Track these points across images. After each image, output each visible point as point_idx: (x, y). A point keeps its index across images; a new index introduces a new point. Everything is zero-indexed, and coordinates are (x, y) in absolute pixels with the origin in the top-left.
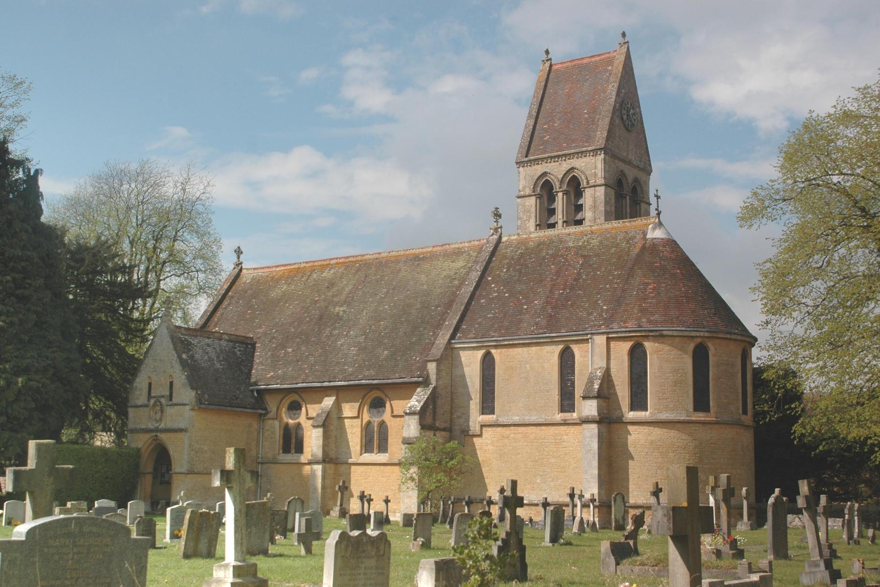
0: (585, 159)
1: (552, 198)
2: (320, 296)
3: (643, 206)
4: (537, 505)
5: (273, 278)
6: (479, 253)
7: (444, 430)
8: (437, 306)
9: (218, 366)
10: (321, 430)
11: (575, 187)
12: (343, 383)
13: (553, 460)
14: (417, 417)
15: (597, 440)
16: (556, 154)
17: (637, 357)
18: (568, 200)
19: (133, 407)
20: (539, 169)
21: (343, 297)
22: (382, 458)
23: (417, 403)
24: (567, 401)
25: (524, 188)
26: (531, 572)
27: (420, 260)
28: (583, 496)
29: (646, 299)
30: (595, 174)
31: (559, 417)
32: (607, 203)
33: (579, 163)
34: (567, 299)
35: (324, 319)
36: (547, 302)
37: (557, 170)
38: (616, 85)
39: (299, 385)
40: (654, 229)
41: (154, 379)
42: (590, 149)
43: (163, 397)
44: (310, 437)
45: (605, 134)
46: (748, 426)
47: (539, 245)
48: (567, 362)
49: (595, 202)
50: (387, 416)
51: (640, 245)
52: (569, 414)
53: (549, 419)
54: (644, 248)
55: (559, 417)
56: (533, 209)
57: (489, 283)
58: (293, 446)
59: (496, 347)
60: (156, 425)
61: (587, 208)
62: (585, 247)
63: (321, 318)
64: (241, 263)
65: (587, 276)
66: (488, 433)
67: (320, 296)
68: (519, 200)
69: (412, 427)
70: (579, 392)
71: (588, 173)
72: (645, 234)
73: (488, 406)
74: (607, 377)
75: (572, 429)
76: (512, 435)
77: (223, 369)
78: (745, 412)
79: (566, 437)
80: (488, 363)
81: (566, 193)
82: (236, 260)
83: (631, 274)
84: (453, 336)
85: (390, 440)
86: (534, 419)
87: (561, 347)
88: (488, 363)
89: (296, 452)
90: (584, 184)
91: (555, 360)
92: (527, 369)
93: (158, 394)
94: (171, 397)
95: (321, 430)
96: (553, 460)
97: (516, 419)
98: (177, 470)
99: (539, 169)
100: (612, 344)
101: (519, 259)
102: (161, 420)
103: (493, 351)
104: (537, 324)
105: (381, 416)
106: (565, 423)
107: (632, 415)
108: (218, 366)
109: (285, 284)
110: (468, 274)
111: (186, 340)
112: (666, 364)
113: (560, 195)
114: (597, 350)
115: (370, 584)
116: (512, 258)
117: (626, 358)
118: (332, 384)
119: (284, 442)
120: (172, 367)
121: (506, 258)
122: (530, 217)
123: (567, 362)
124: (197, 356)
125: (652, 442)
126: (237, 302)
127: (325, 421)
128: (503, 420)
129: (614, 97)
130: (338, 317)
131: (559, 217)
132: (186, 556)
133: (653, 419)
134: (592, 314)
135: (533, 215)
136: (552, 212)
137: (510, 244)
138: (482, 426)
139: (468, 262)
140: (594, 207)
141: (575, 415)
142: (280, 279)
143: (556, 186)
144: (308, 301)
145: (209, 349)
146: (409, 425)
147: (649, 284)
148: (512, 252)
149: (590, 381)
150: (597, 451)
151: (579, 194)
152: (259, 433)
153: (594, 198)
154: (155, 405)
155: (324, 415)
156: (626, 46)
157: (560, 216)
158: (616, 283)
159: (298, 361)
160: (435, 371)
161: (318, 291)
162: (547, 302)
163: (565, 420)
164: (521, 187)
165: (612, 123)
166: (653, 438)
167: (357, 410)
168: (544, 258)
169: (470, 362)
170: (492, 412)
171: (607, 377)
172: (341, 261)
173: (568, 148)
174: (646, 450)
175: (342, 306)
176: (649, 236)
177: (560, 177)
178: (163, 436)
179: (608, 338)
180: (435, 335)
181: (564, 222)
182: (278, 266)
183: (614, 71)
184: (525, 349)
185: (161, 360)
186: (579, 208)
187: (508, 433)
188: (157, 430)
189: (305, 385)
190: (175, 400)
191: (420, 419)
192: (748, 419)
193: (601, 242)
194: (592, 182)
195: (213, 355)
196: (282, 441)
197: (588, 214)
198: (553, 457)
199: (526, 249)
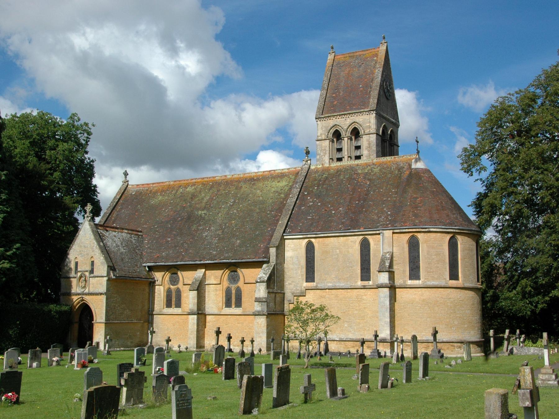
0: (362, 117)
2: (186, 203)
3: (395, 147)
4: (101, 294)
5: (151, 191)
6: (296, 176)
8: (271, 211)
9: (122, 250)
10: (196, 292)
11: (356, 133)
12: (210, 262)
13: (356, 312)
14: (265, 284)
15: (388, 299)
16: (343, 113)
17: (414, 245)
19: (64, 278)
20: (331, 122)
21: (203, 205)
22: (238, 311)
23: (264, 275)
24: (366, 274)
25: (321, 134)
27: (255, 180)
28: (378, 336)
29: (417, 207)
30: (370, 127)
32: (377, 145)
34: (362, 206)
35: (191, 218)
36: (348, 209)
37: (344, 123)
38: (381, 69)
39: (179, 263)
40: (416, 161)
41: (79, 260)
42: (366, 110)
43: (87, 271)
44: (187, 297)
45: (376, 101)
47: (338, 172)
48: (365, 247)
49: (369, 144)
51: (408, 172)
52: (367, 282)
53: (354, 285)
54: (410, 174)
55: (360, 283)
56: (328, 149)
58: (173, 303)
60: (83, 290)
61: (364, 148)
62: (370, 174)
63: (189, 218)
64: (128, 181)
65: (374, 192)
67: (186, 203)
68: (318, 142)
69: (262, 291)
70: (374, 266)
71: (364, 126)
72: (410, 165)
73: (310, 275)
75: (369, 292)
76: (327, 296)
77: (125, 253)
79: (365, 297)
80: (310, 248)
82: (124, 179)
83: (404, 191)
85: (244, 299)
86: (342, 285)
88: (310, 248)
89: (176, 307)
90: (361, 132)
91: (357, 247)
93: (83, 269)
94: (92, 271)
95: (196, 292)
96: (356, 312)
97: (330, 285)
98: (98, 321)
101: (325, 181)
102: (85, 287)
103: (313, 240)
104: (343, 223)
105: (237, 283)
106: (364, 288)
107: (410, 282)
108: (122, 250)
109: (161, 195)
110: (290, 189)
111: (101, 233)
113: (346, 139)
114: (386, 241)
116: (320, 180)
118: (202, 262)
119: (167, 301)
120: (93, 251)
121: (316, 180)
122: (325, 153)
123: (365, 247)
124: (109, 244)
125: (424, 300)
126: (127, 207)
127: (198, 287)
128: (320, 286)
129: (380, 77)
130: (201, 218)
131: (345, 153)
134: (380, 217)
135: (328, 152)
136: (340, 150)
137: (317, 171)
139: (289, 182)
140: (369, 147)
141: (371, 283)
142: (156, 192)
143: (343, 134)
144: (178, 207)
145: (116, 239)
146: (259, 290)
147: (417, 198)
148: (319, 176)
149: (383, 261)
150: (389, 306)
152: (149, 294)
153: (369, 142)
154: (81, 277)
155: (198, 283)
156: (386, 44)
157: (346, 153)
158: (395, 197)
159: (176, 247)
160: (275, 254)
161: (185, 200)
162: (348, 209)
163: (364, 286)
164: (319, 134)
165: (379, 94)
166: (424, 298)
167: (219, 280)
168: (342, 180)
169: (295, 249)
170: (313, 281)
172: (199, 180)
173: (351, 110)
174: (420, 305)
175: (203, 210)
176: (413, 166)
177: (346, 128)
178: (88, 298)
179: (393, 233)
180: (273, 231)
181: (349, 157)
182: (154, 184)
183: (379, 61)
185: (85, 247)
187: (324, 294)
188: (83, 294)
189: (182, 263)
190: (96, 273)
191: (267, 284)
193: (380, 170)
194: (367, 131)
195: (119, 244)
196: (165, 300)
197: (364, 152)
198: (356, 310)
199: (329, 174)
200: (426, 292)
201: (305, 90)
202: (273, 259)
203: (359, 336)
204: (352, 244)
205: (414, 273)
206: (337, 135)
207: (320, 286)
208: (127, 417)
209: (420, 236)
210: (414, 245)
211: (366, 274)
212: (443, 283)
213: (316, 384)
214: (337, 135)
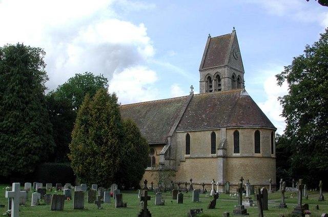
1: (211, 82)
7: (173, 160)
11: (218, 78)
17: (236, 135)
18: (216, 83)
20: (207, 72)
24: (213, 151)
26: (217, 206)
31: (211, 155)
33: (219, 70)
37: (212, 73)
46: (274, 158)
48: (213, 136)
50: (155, 155)
53: (208, 156)
55: (211, 155)
57: (189, 111)
59: (190, 132)
66: (188, 161)
70: (217, 148)
73: (188, 152)
74: (226, 142)
75: (215, 159)
78: (272, 153)
80: (188, 137)
81: (215, 80)
84: (176, 128)
86: (202, 156)
87: (211, 132)
88: (188, 137)
92: (202, 138)
97: (197, 156)
99: (207, 72)
100: (228, 130)
103: (189, 133)
106: (212, 157)
107: (234, 155)
112: (247, 137)
113: (213, 81)
115: (254, 216)
117: (233, 136)
123: (213, 136)
131: (213, 88)
132: (52, 210)
133: (242, 156)
136: (211, 86)
138: (186, 158)
140: (225, 85)
141: (216, 155)
151: (220, 80)
153: (225, 82)
169: (181, 137)
171: (226, 142)
184: (200, 133)
186: (220, 85)
192: (273, 156)
194: (224, 77)
197: (222, 87)
200: (243, 160)
201: (13, 47)
202: (169, 142)
203: (202, 182)
204: (208, 135)
205: (237, 150)
206: (209, 78)
207: (192, 157)
208: (84, 213)
209: (240, 131)
210: (236, 135)
211: (213, 151)
212: (251, 155)
213: (133, 200)
214: (209, 78)
